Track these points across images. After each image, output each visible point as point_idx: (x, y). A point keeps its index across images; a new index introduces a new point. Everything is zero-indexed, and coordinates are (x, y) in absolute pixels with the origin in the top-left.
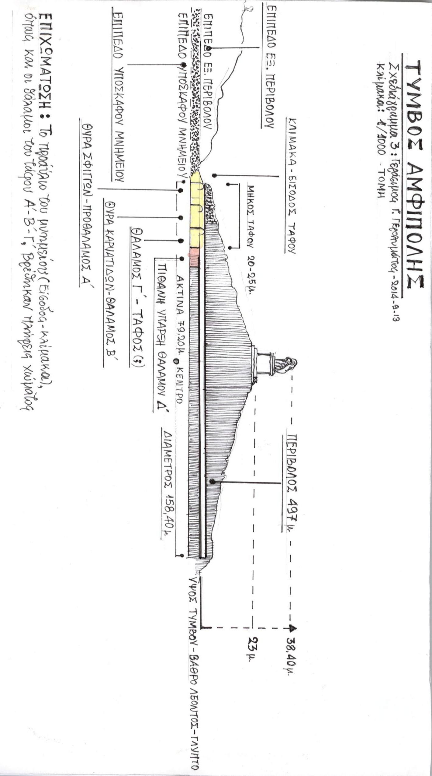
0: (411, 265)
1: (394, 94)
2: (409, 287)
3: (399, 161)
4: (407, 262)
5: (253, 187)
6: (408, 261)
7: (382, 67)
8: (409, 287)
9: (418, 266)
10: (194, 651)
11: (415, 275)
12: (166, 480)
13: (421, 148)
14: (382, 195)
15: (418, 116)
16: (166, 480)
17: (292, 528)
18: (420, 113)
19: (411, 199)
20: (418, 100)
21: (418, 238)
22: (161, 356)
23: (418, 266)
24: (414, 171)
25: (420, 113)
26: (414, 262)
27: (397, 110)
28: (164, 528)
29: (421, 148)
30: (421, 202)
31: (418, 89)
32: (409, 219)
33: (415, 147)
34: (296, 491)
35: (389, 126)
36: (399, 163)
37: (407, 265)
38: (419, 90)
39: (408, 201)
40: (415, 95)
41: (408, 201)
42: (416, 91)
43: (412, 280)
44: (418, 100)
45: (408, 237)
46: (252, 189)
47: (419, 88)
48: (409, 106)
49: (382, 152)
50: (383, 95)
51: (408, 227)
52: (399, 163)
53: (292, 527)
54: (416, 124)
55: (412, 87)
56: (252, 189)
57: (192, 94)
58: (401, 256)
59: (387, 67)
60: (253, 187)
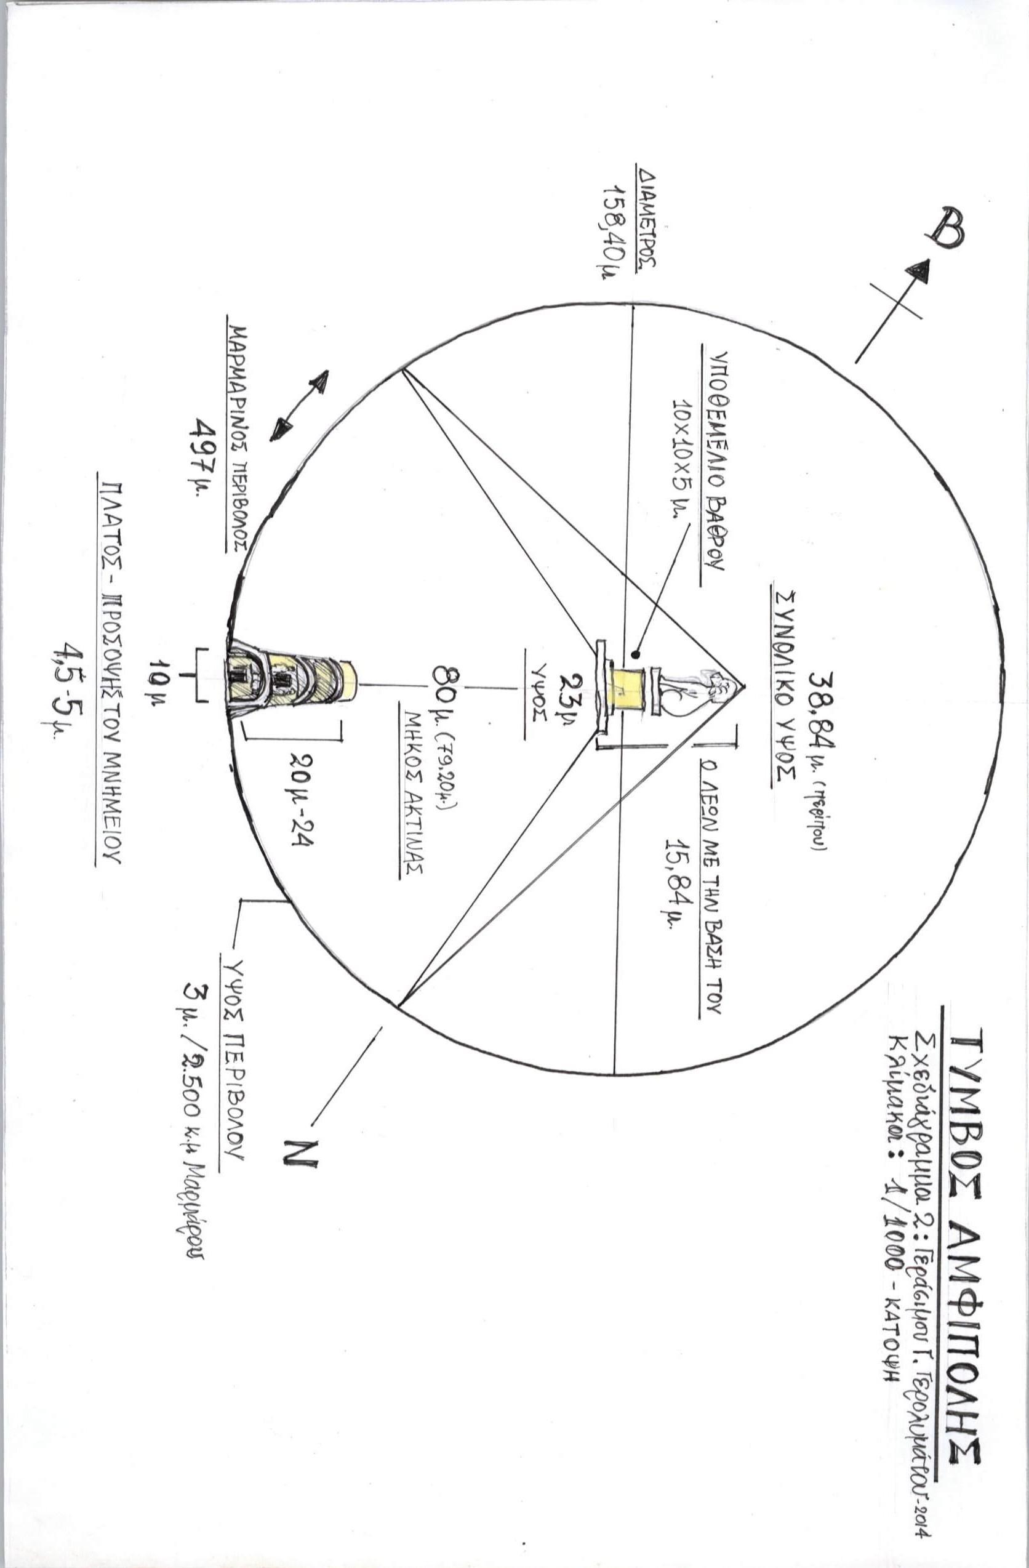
0: (954, 1422)
1: (924, 1104)
2: (953, 1193)
3: (932, 1251)
4: (949, 1340)
6: (949, 1413)
7: (901, 1044)
8: (953, 1193)
9: (969, 1423)
10: (525, 650)
11: (963, 1441)
12: (235, 438)
13: (978, 1195)
15: (974, 1131)
16: (235, 438)
20: (975, 1100)
21: (970, 1375)
22: (720, 398)
23: (969, 1423)
26: (961, 1415)
27: (927, 1274)
29: (978, 1195)
30: (976, 1304)
32: (952, 1337)
33: (965, 1193)
35: (914, 1163)
37: (946, 1421)
39: (950, 1303)
40: (970, 1093)
41: (950, 1303)
42: (970, 1084)
43: (957, 1182)
44: (975, 1100)
45: (953, 1156)
48: (954, 1110)
50: (902, 1114)
54: (971, 1145)
58: (938, 1112)
59: (910, 1043)
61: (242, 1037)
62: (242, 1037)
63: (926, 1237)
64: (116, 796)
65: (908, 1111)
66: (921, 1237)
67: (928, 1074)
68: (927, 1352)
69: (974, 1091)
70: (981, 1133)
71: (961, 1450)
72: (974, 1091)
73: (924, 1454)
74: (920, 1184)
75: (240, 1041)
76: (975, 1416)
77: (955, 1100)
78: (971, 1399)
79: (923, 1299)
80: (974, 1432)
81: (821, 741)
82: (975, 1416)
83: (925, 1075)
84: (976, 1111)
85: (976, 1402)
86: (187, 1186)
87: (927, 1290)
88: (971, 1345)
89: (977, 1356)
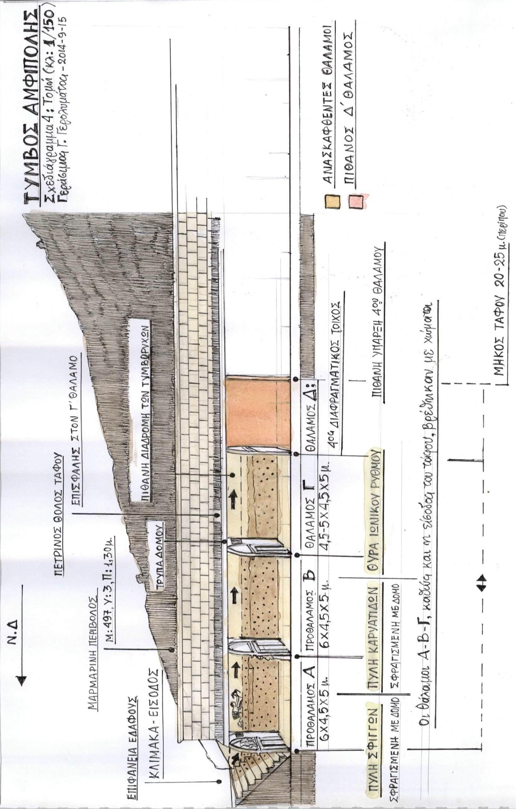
0: (34, 27)
5: (393, 616)
9: (28, 27)
14: (92, 653)
17: (323, 682)
18: (25, 157)
19: (34, 83)
23: (28, 27)
24: (32, 106)
25: (25, 157)
26: (32, 30)
28: (505, 252)
30: (26, 80)
31: (26, 180)
34: (308, 685)
36: (43, 98)
38: (26, 178)
39: (37, 81)
41: (37, 81)
46: (394, 614)
47: (25, 180)
49: (73, 359)
51: (36, 61)
52: (43, 98)
53: (323, 683)
55: (33, 113)
56: (394, 614)
57: (423, 311)
58: (41, 32)
60: (393, 616)
61: (346, 182)
62: (346, 182)
63: (108, 631)
64: (348, 63)
65: (57, 166)
66: (110, 631)
67: (47, 183)
68: (60, 145)
69: (27, 173)
70: (24, 155)
71: (33, 15)
72: (27, 173)
73: (60, 95)
74: (50, 133)
75: (347, 180)
76: (25, 30)
77: (36, 169)
78: (27, 39)
79: (61, 173)
80: (25, 24)
81: (62, 47)
82: (25, 30)
83: (48, 183)
84: (26, 164)
85: (25, 37)
86: (431, 523)
87: (60, 178)
88: (27, 63)
89: (24, 59)
